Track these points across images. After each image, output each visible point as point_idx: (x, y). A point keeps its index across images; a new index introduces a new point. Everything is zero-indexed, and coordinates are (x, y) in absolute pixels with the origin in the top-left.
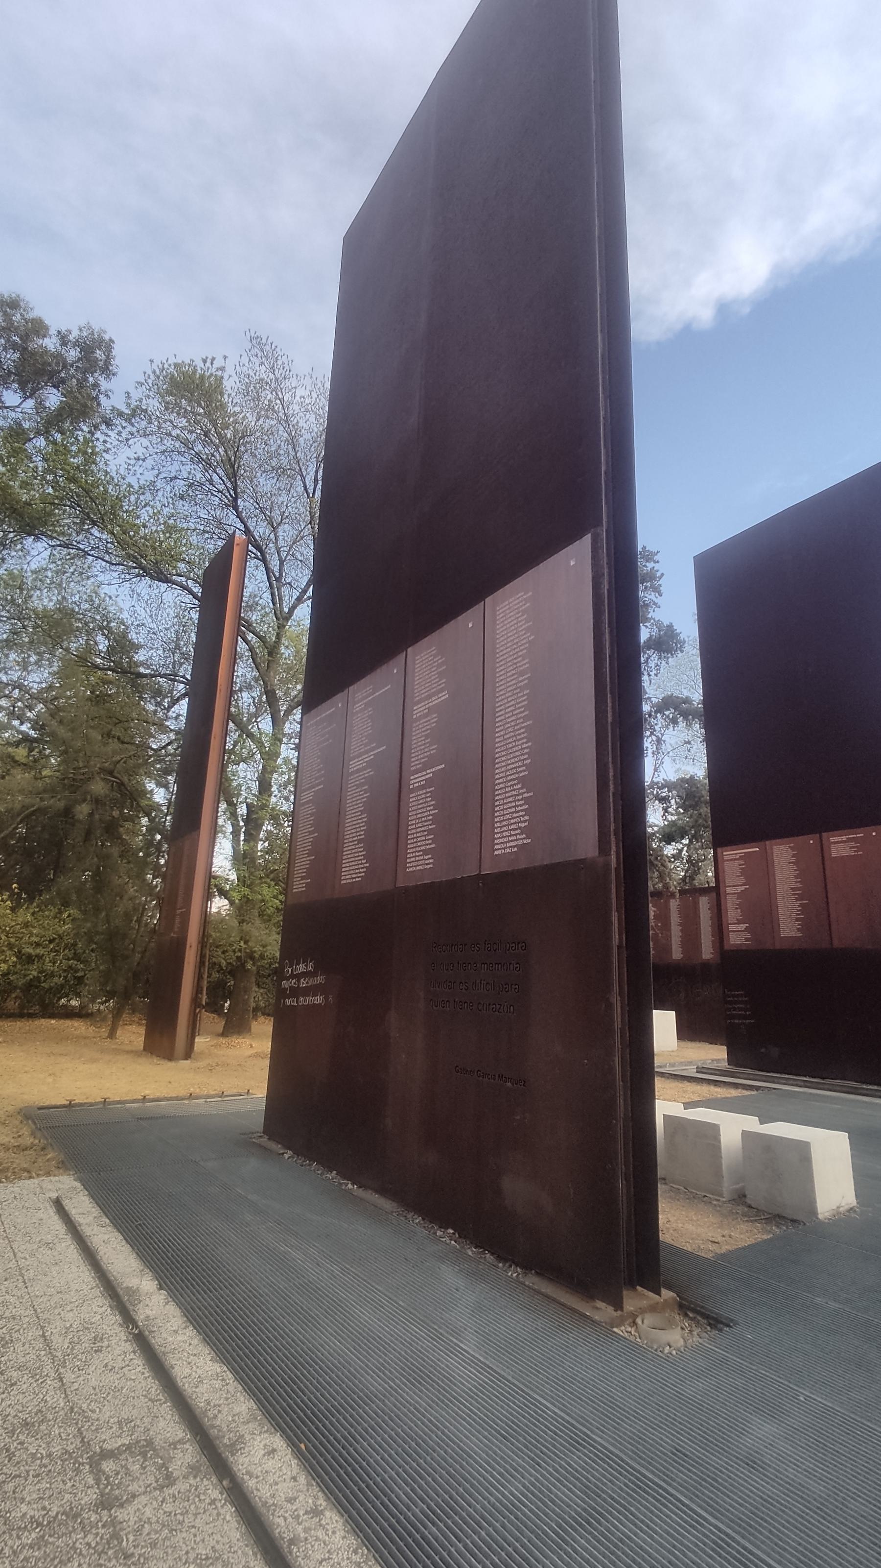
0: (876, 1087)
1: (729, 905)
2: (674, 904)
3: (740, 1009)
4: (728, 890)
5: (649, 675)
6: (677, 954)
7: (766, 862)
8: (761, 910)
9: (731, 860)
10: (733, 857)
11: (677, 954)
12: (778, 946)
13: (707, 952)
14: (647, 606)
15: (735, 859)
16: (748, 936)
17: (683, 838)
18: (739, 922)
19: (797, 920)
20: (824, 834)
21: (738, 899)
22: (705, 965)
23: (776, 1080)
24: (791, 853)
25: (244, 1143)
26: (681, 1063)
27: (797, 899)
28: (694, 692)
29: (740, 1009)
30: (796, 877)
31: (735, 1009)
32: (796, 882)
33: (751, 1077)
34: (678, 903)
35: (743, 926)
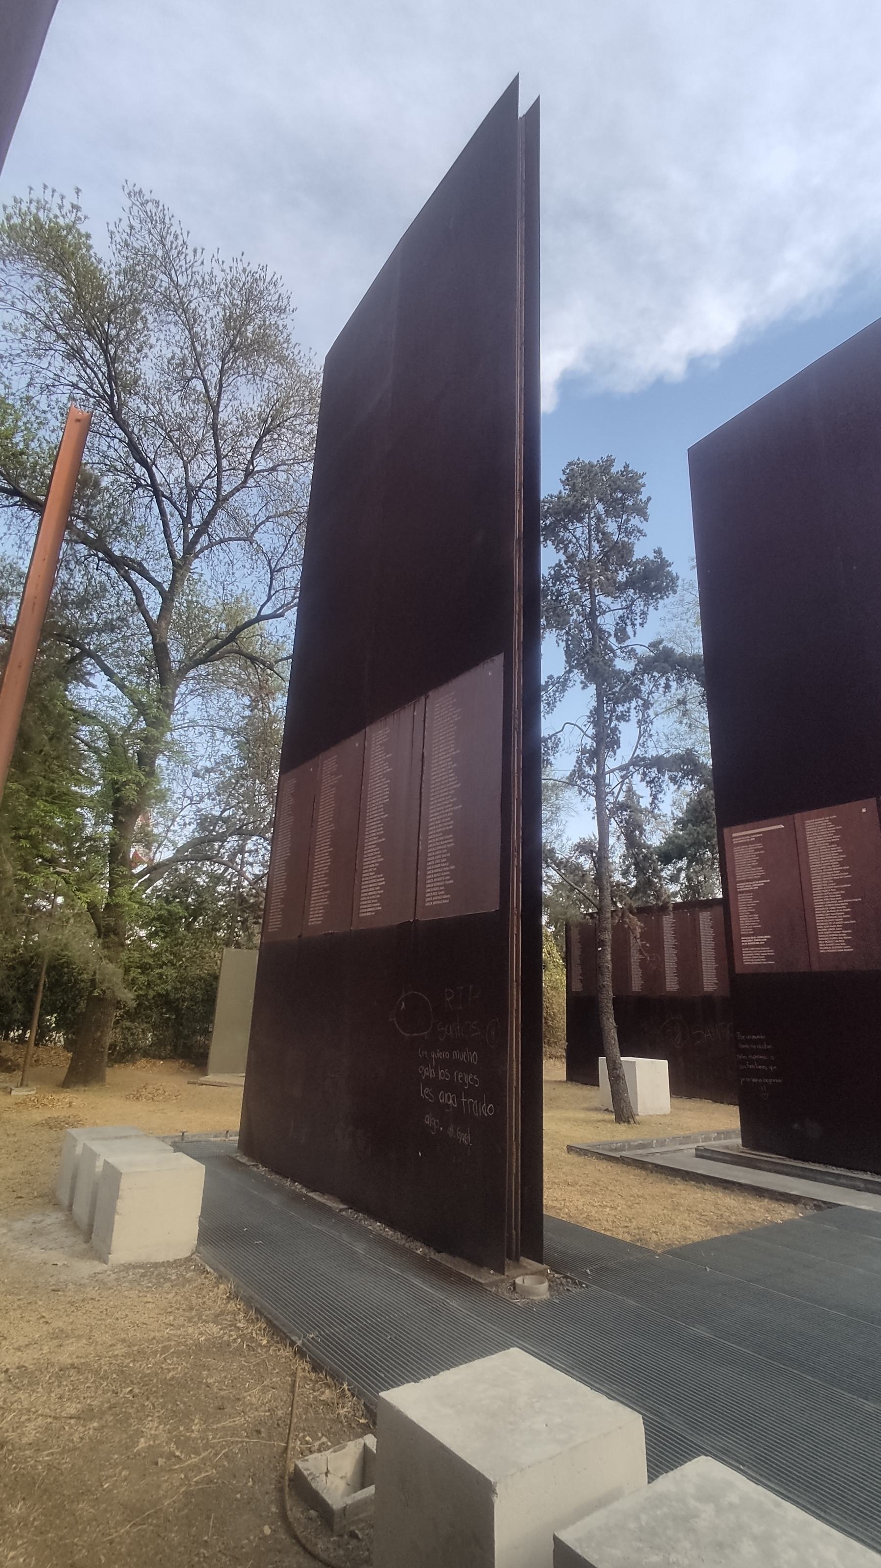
1: (742, 909)
2: (668, 921)
3: (760, 1062)
4: (741, 887)
5: (633, 625)
6: (671, 984)
8: (790, 915)
9: (744, 844)
11: (671, 984)
12: (816, 967)
13: (710, 981)
16: (771, 952)
19: (845, 927)
21: (754, 899)
22: (708, 999)
23: (818, 1177)
27: (844, 897)
28: (691, 642)
29: (760, 1062)
30: (841, 864)
31: (751, 1062)
32: (842, 871)
33: (778, 1168)
34: (672, 921)
35: (762, 939)
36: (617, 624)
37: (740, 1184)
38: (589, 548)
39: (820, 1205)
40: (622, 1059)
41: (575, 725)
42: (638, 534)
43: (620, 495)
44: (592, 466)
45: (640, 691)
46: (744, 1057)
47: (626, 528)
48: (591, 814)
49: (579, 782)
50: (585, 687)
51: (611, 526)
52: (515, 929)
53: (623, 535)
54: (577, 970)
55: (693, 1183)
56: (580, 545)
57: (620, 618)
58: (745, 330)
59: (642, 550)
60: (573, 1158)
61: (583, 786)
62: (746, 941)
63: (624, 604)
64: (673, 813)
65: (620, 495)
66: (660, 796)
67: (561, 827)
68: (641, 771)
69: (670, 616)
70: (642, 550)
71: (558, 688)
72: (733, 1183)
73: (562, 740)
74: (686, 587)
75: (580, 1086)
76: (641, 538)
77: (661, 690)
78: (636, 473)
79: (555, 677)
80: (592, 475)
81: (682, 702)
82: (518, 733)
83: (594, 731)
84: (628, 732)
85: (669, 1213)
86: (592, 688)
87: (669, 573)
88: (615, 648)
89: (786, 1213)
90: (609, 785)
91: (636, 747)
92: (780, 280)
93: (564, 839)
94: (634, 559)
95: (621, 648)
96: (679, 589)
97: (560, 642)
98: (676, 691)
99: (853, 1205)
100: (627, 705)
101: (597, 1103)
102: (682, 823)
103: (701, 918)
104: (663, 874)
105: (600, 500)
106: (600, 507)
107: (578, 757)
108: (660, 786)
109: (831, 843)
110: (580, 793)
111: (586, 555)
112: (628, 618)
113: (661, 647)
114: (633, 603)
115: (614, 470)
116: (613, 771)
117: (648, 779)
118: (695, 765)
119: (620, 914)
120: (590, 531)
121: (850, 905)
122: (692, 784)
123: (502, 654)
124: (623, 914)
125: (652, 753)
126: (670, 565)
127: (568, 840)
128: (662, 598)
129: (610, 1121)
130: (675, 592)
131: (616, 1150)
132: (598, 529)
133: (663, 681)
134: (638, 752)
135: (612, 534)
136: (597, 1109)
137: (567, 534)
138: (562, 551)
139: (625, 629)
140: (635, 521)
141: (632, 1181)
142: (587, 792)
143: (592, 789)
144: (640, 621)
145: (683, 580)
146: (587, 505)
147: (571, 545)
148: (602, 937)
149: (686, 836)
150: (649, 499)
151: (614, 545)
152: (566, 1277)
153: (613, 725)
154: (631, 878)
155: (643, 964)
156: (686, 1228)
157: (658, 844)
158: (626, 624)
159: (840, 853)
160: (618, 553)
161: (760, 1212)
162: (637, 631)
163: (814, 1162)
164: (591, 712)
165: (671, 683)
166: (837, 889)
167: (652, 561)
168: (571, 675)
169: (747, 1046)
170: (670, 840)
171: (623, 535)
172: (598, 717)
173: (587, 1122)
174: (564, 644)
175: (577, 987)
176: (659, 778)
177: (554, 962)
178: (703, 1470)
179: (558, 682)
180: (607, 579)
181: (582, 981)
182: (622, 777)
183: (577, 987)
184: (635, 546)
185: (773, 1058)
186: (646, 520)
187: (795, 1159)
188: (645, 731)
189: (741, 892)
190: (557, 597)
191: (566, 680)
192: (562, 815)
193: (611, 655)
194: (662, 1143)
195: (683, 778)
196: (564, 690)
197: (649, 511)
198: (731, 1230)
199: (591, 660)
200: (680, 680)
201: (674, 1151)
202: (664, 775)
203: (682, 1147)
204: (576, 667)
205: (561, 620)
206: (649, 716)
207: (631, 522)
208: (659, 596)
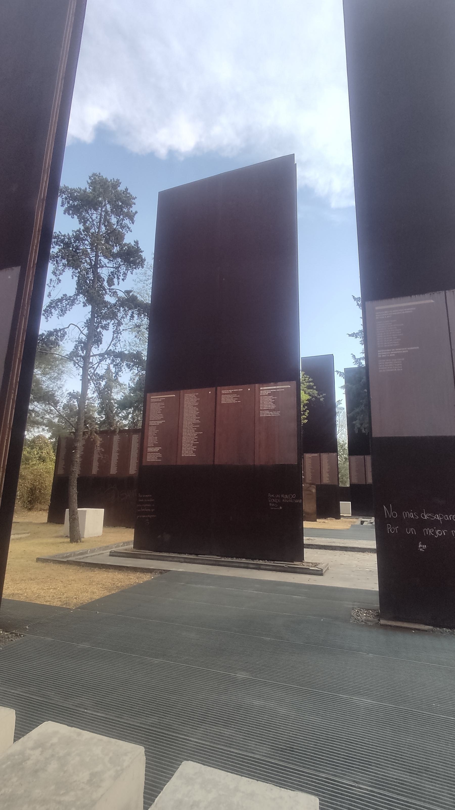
0: (453, 718)
1: (150, 433)
4: (151, 423)
7: (179, 403)
8: (171, 438)
9: (156, 402)
10: (158, 400)
11: (113, 471)
12: (179, 463)
13: (133, 470)
14: (138, 443)
15: (157, 402)
17: (130, 408)
18: (155, 446)
19: (194, 445)
20: (219, 388)
21: (156, 429)
22: (131, 478)
24: (196, 399)
25: (47, 523)
26: (100, 549)
27: (196, 431)
28: (145, 295)
30: (197, 416)
32: (197, 419)
35: (157, 449)
36: (109, 275)
37: (127, 567)
38: (99, 228)
39: (162, 572)
40: (78, 509)
41: (76, 326)
42: (128, 229)
43: (120, 204)
44: (107, 181)
45: (117, 316)
46: (140, 506)
47: (121, 224)
48: (80, 378)
49: (74, 358)
50: (85, 305)
51: (114, 220)
52: (6, 436)
53: (119, 227)
54: (62, 463)
55: (104, 569)
56: (94, 224)
57: (111, 272)
58: (198, 147)
59: (129, 239)
60: (40, 564)
61: (77, 361)
62: (150, 449)
63: (115, 265)
64: (129, 384)
65: (120, 204)
66: (120, 373)
67: (62, 383)
68: (111, 359)
69: (138, 280)
70: (129, 239)
71: (69, 302)
72: (124, 567)
73: (67, 333)
74: (149, 267)
75: (55, 525)
76: (129, 232)
77: (128, 317)
78: (131, 195)
79: (68, 296)
80: (106, 186)
81: (139, 326)
82: (25, 319)
83: (87, 332)
84: (107, 336)
85: (86, 587)
86: (89, 308)
87: (141, 256)
88: (106, 288)
89: (146, 577)
90: (92, 363)
91: (110, 345)
92: (216, 130)
93: (64, 389)
94: (124, 243)
95: (109, 289)
96: (145, 266)
97: (74, 276)
98: (136, 320)
99: (176, 570)
100: (109, 321)
101: (62, 534)
102: (133, 390)
103: (133, 437)
104: (120, 415)
105: (109, 202)
106: (108, 207)
107: (76, 345)
108: (121, 368)
109: (194, 406)
110: (75, 366)
111: (97, 231)
112: (116, 274)
113: (131, 294)
114: (119, 267)
115: (119, 189)
116: (95, 355)
117: (115, 363)
118: (140, 360)
119: (89, 433)
120: (100, 219)
121: (198, 435)
122: (138, 370)
123: (20, 267)
124: (91, 433)
125: (118, 350)
126: (142, 252)
127: (66, 391)
128: (135, 268)
129: (67, 542)
130: (143, 267)
131: (67, 557)
132: (105, 220)
133: (130, 313)
134: (111, 348)
135: (114, 225)
136: (62, 537)
137: (87, 215)
138: (82, 224)
139: (112, 279)
140: (127, 221)
141: (71, 573)
142: (79, 365)
143: (81, 364)
144: (123, 278)
145: (148, 263)
146: (101, 203)
147: (88, 222)
148: (76, 445)
149: (134, 397)
150: (136, 212)
151: (113, 231)
152: (12, 633)
153: (98, 330)
154: (103, 416)
155: (99, 460)
156: (94, 593)
157: (120, 399)
158: (114, 277)
159: (197, 411)
160: (115, 236)
161: (133, 579)
162: (120, 282)
163: (165, 552)
164: (87, 321)
165: (134, 315)
166: (194, 428)
167: (133, 247)
168: (78, 297)
169: (142, 500)
170: (126, 398)
171: (119, 227)
172: (90, 324)
173: (53, 544)
174: (76, 278)
175: (61, 472)
176: (121, 364)
177: (50, 458)
178: (49, 729)
179: (70, 299)
180: (106, 248)
181: (64, 468)
182: (100, 360)
183: (61, 472)
184: (126, 236)
185: (153, 505)
186: (133, 223)
187: (157, 551)
188: (117, 337)
189: (151, 426)
190: (76, 249)
191: (74, 299)
192: (65, 376)
193: (104, 292)
194: (93, 551)
195: (133, 366)
196: (72, 305)
197: (135, 219)
198: (117, 590)
199: (91, 290)
200: (139, 315)
201: (99, 554)
202: (123, 363)
203: (103, 552)
204: (81, 293)
205: (75, 263)
206: (120, 330)
207: (124, 221)
208: (134, 267)
